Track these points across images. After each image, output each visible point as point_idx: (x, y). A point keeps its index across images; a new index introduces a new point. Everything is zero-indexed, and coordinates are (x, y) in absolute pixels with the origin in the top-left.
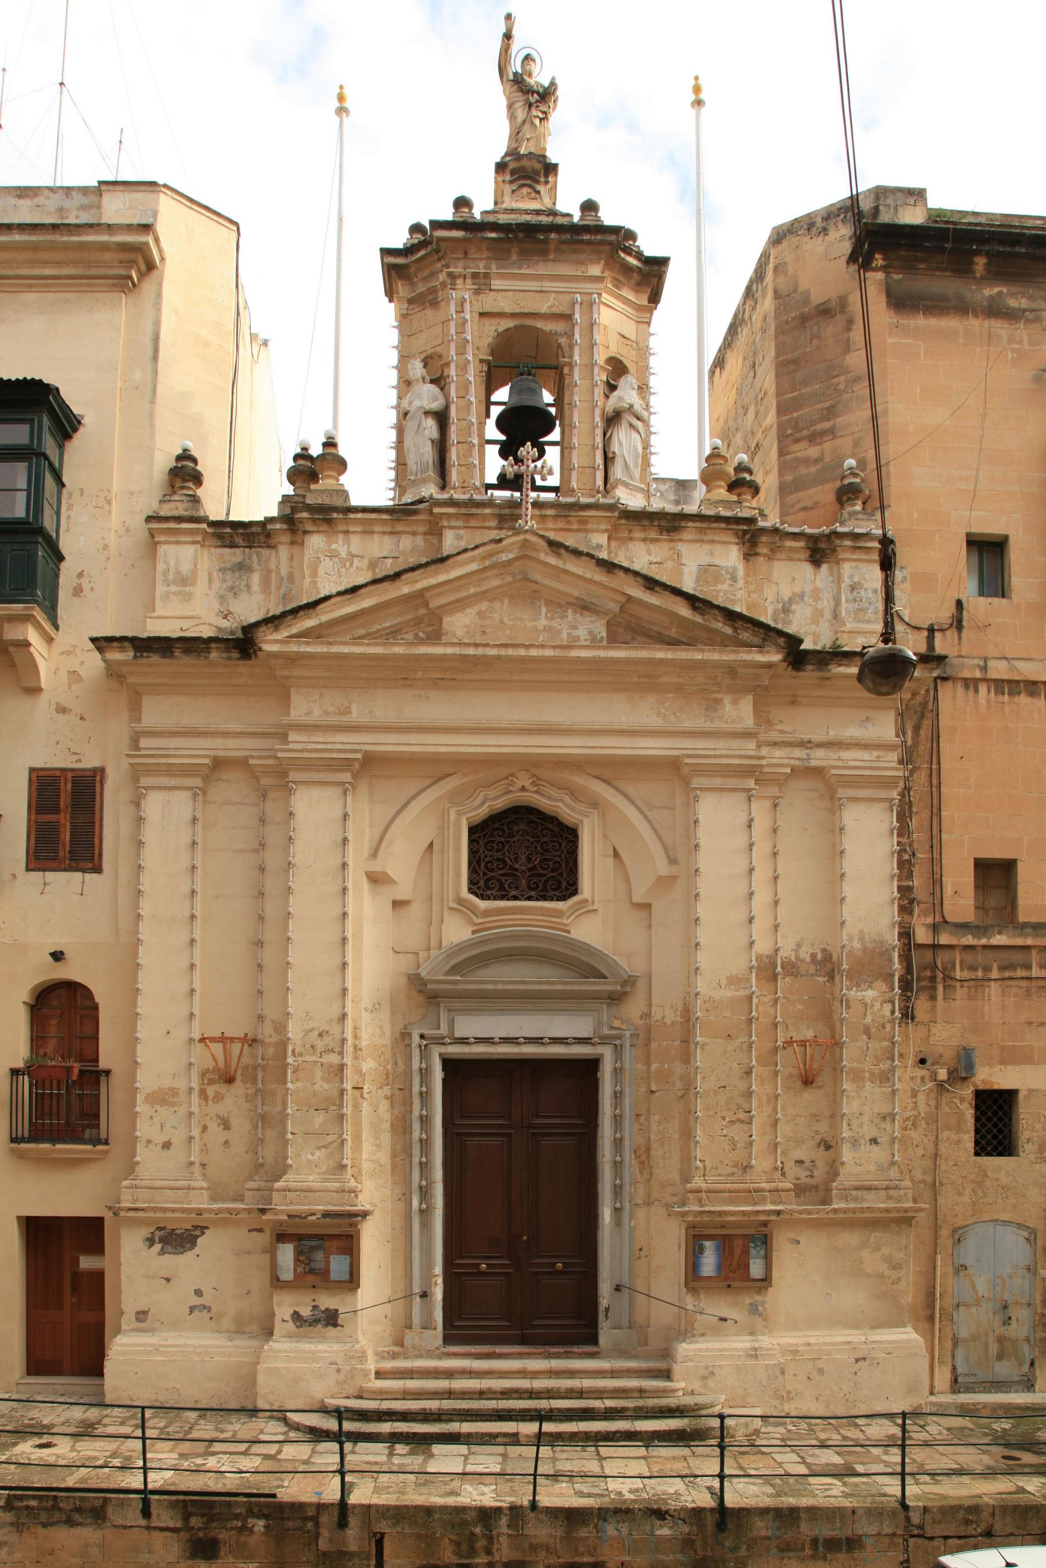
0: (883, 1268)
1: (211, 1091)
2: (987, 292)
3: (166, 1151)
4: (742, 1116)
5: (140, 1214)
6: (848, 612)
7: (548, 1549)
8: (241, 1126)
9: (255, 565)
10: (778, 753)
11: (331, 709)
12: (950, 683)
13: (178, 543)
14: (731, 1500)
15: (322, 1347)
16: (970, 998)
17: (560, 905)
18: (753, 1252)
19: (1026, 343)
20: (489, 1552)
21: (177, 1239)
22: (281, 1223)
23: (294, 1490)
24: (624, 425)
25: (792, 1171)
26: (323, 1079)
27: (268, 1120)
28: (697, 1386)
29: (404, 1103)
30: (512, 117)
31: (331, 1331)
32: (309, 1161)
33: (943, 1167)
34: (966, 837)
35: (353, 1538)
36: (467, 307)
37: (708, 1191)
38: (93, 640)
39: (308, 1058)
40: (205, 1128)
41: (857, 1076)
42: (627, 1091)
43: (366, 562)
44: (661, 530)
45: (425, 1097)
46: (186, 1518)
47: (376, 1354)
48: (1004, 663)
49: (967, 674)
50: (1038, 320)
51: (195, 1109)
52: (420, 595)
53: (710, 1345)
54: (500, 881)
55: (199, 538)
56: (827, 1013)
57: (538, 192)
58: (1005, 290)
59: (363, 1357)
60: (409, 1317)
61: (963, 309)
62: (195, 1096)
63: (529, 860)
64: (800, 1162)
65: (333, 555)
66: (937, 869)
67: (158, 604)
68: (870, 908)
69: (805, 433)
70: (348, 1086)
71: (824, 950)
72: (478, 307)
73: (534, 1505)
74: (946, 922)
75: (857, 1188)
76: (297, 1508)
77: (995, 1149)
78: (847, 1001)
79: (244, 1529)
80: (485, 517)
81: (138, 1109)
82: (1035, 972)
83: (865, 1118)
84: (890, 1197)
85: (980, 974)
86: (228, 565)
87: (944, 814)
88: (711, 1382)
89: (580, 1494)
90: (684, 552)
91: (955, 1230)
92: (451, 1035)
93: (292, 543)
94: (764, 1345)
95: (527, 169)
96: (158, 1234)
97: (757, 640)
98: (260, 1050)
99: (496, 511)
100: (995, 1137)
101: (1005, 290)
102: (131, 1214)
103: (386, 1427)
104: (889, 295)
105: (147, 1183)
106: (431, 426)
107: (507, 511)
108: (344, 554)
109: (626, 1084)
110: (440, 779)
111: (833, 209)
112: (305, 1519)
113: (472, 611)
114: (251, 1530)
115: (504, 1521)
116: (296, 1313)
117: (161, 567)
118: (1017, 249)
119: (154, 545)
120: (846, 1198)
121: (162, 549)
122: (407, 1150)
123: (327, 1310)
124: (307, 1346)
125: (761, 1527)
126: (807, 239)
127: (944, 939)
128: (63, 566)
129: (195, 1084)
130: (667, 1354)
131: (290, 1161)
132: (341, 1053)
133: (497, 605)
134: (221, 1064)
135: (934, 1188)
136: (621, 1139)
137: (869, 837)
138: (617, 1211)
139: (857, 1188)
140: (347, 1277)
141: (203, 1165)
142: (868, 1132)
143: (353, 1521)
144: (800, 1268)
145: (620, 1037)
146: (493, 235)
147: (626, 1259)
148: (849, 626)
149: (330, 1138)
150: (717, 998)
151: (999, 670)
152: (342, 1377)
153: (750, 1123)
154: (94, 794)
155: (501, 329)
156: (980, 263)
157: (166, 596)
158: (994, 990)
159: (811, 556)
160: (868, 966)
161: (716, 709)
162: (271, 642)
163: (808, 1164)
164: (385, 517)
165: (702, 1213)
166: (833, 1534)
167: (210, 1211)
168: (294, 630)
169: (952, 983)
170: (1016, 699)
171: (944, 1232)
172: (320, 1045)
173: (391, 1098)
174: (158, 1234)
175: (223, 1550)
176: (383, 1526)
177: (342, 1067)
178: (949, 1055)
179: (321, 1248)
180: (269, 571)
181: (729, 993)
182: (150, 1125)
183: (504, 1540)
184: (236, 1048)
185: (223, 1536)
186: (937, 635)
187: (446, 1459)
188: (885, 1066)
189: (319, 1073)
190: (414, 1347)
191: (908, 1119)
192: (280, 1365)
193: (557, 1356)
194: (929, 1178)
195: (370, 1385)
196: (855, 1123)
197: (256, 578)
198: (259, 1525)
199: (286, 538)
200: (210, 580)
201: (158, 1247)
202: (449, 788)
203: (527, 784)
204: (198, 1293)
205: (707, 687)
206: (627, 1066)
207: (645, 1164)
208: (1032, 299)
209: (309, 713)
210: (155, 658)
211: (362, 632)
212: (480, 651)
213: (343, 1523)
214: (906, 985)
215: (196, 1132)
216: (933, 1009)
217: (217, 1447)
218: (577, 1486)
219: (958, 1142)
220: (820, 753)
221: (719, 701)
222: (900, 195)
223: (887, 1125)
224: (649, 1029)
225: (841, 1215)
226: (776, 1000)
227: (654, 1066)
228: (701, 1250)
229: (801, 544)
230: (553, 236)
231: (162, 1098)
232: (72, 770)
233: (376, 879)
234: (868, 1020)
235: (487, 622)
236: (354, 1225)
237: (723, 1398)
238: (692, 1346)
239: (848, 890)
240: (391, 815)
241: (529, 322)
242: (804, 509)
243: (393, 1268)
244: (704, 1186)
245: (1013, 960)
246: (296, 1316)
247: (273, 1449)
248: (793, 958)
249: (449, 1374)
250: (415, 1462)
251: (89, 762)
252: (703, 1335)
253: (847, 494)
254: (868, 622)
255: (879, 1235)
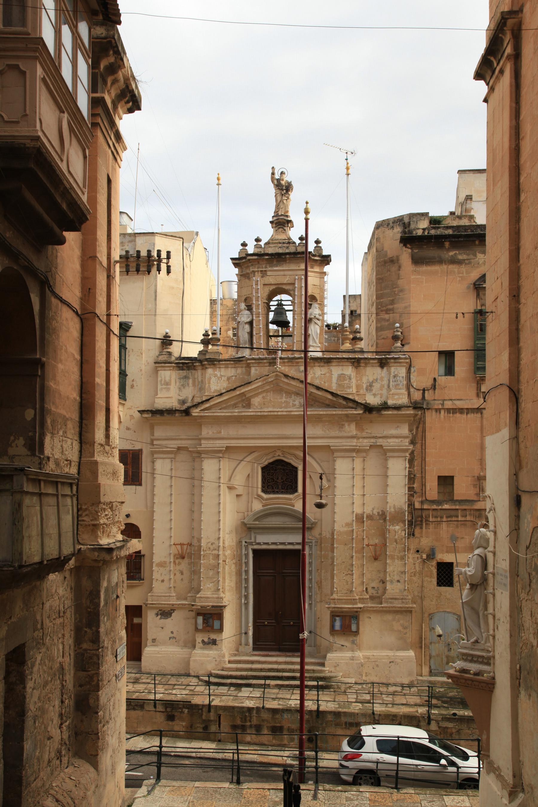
0: (400, 628)
1: (177, 561)
2: (451, 253)
3: (162, 583)
4: (350, 572)
5: (154, 606)
6: (393, 386)
7: (267, 721)
8: (186, 573)
9: (190, 377)
10: (365, 441)
11: (215, 432)
12: (430, 411)
13: (165, 370)
14: (322, 708)
15: (211, 652)
16: (435, 528)
17: (291, 496)
18: (353, 621)
19: (465, 273)
20: (250, 721)
21: (165, 613)
22: (199, 609)
23: (197, 700)
24: (313, 323)
25: (370, 591)
26: (213, 559)
27: (195, 572)
28: (333, 669)
29: (240, 565)
30: (276, 200)
31: (214, 647)
32: (208, 587)
33: (425, 591)
34: (435, 468)
35: (212, 716)
36: (259, 283)
37: (338, 599)
38: (139, 411)
39: (208, 552)
40: (175, 574)
41: (392, 558)
42: (313, 562)
43: (226, 378)
44: (325, 363)
45: (247, 564)
46: (166, 709)
47: (230, 654)
48: (451, 402)
49: (436, 407)
50: (470, 263)
51: (172, 569)
52: (243, 394)
53: (338, 655)
54: (272, 486)
55: (172, 368)
56: (383, 533)
57: (285, 230)
58: (457, 252)
59: (224, 656)
60: (241, 641)
61: (441, 261)
62: (172, 564)
63: (282, 479)
64: (373, 588)
65: (215, 376)
66: (424, 480)
67: (159, 392)
68: (397, 495)
69: (384, 308)
70: (221, 561)
71: (382, 511)
72: (263, 282)
73: (263, 707)
74: (427, 500)
75: (391, 599)
76: (197, 706)
77: (447, 584)
78: (389, 530)
79: (182, 712)
80: (264, 363)
81: (154, 569)
82: (460, 518)
83: (395, 573)
84: (403, 602)
85: (439, 519)
86: (181, 377)
87: (426, 459)
88: (338, 668)
89: (279, 704)
90: (333, 370)
91: (430, 615)
92: (255, 542)
93: (202, 369)
94: (356, 655)
95: (281, 222)
96: (160, 612)
97: (354, 406)
98: (193, 548)
99: (268, 361)
100: (447, 579)
101: (457, 252)
102: (151, 605)
103: (229, 681)
104: (412, 259)
105: (156, 594)
106: (247, 327)
107: (272, 361)
108: (219, 376)
109: (313, 559)
110: (251, 453)
111: (396, 219)
112: (199, 709)
113: (261, 396)
114: (184, 712)
115: (255, 712)
116: (203, 640)
117: (159, 379)
118: (460, 239)
119: (156, 371)
120: (387, 602)
121: (160, 372)
122: (241, 581)
123: (213, 639)
124: (206, 652)
125: (330, 718)
126: (387, 229)
127: (425, 506)
128: (127, 377)
129: (172, 560)
130: (325, 657)
131: (202, 588)
132: (218, 550)
133: (269, 394)
134: (180, 552)
135: (422, 598)
136: (312, 579)
137: (398, 469)
138: (310, 604)
139: (391, 599)
140: (219, 628)
141: (174, 587)
142: (396, 578)
143: (212, 710)
144: (370, 628)
145: (311, 542)
146: (267, 257)
147: (313, 622)
148: (393, 391)
149: (215, 579)
150: (342, 531)
151: (448, 405)
152: (217, 663)
153: (352, 575)
154: (139, 458)
155: (271, 289)
156: (447, 244)
157: (162, 389)
158: (444, 525)
159: (380, 365)
160: (397, 517)
161: (342, 428)
162: (195, 412)
163: (376, 588)
164: (232, 362)
165: (334, 608)
166: (351, 721)
167: (176, 604)
168: (202, 408)
169: (428, 523)
170: (455, 415)
171: (426, 615)
172: (212, 547)
173: (235, 564)
174: (160, 612)
175: (176, 718)
176: (221, 712)
177: (218, 555)
178: (427, 549)
179: (210, 618)
180: (195, 378)
181: (346, 529)
182: (158, 574)
183: (254, 718)
184: (185, 547)
185: (176, 714)
186: (426, 392)
187: (245, 692)
188: (402, 554)
189: (211, 557)
190: (242, 652)
191: (412, 573)
192: (197, 658)
193: (290, 656)
194: (420, 595)
195: (226, 666)
196: (391, 574)
197: (191, 381)
198: (186, 711)
199: (200, 368)
200: (176, 382)
201: (159, 616)
202: (254, 456)
203: (280, 454)
204: (172, 632)
205: (338, 422)
206: (313, 553)
207: (320, 587)
208: (468, 255)
209: (208, 433)
210: (158, 416)
211: (225, 406)
212: (262, 414)
213: (209, 711)
214: (410, 523)
215: (172, 577)
216: (422, 532)
217: (176, 687)
218: (280, 702)
219: (431, 581)
220: (381, 440)
221: (343, 425)
222: (418, 216)
223: (403, 576)
224: (321, 538)
225: (385, 609)
226: (364, 530)
227: (323, 553)
228: (335, 620)
229: (376, 361)
230: (288, 256)
231: (161, 565)
232: (132, 450)
233: (230, 488)
234: (396, 537)
235: (265, 400)
236: (222, 610)
237: (341, 674)
238: (332, 655)
239: (389, 490)
240: (235, 466)
241: (280, 286)
242: (383, 338)
243: (235, 624)
244: (336, 597)
245: (451, 514)
246: (203, 641)
247: (193, 688)
248: (371, 514)
249: (252, 662)
250: (234, 693)
251: (137, 447)
252: (336, 651)
253: (395, 338)
254: (400, 389)
255: (399, 616)
